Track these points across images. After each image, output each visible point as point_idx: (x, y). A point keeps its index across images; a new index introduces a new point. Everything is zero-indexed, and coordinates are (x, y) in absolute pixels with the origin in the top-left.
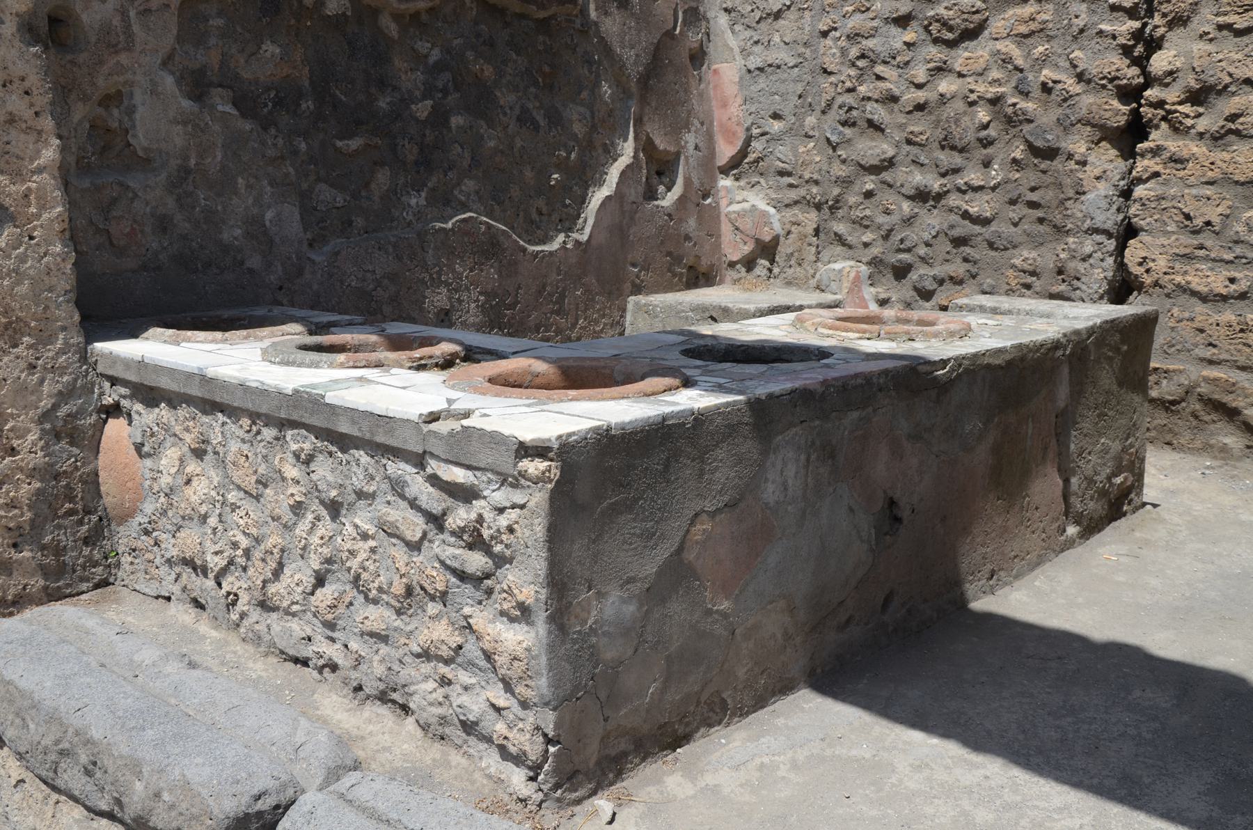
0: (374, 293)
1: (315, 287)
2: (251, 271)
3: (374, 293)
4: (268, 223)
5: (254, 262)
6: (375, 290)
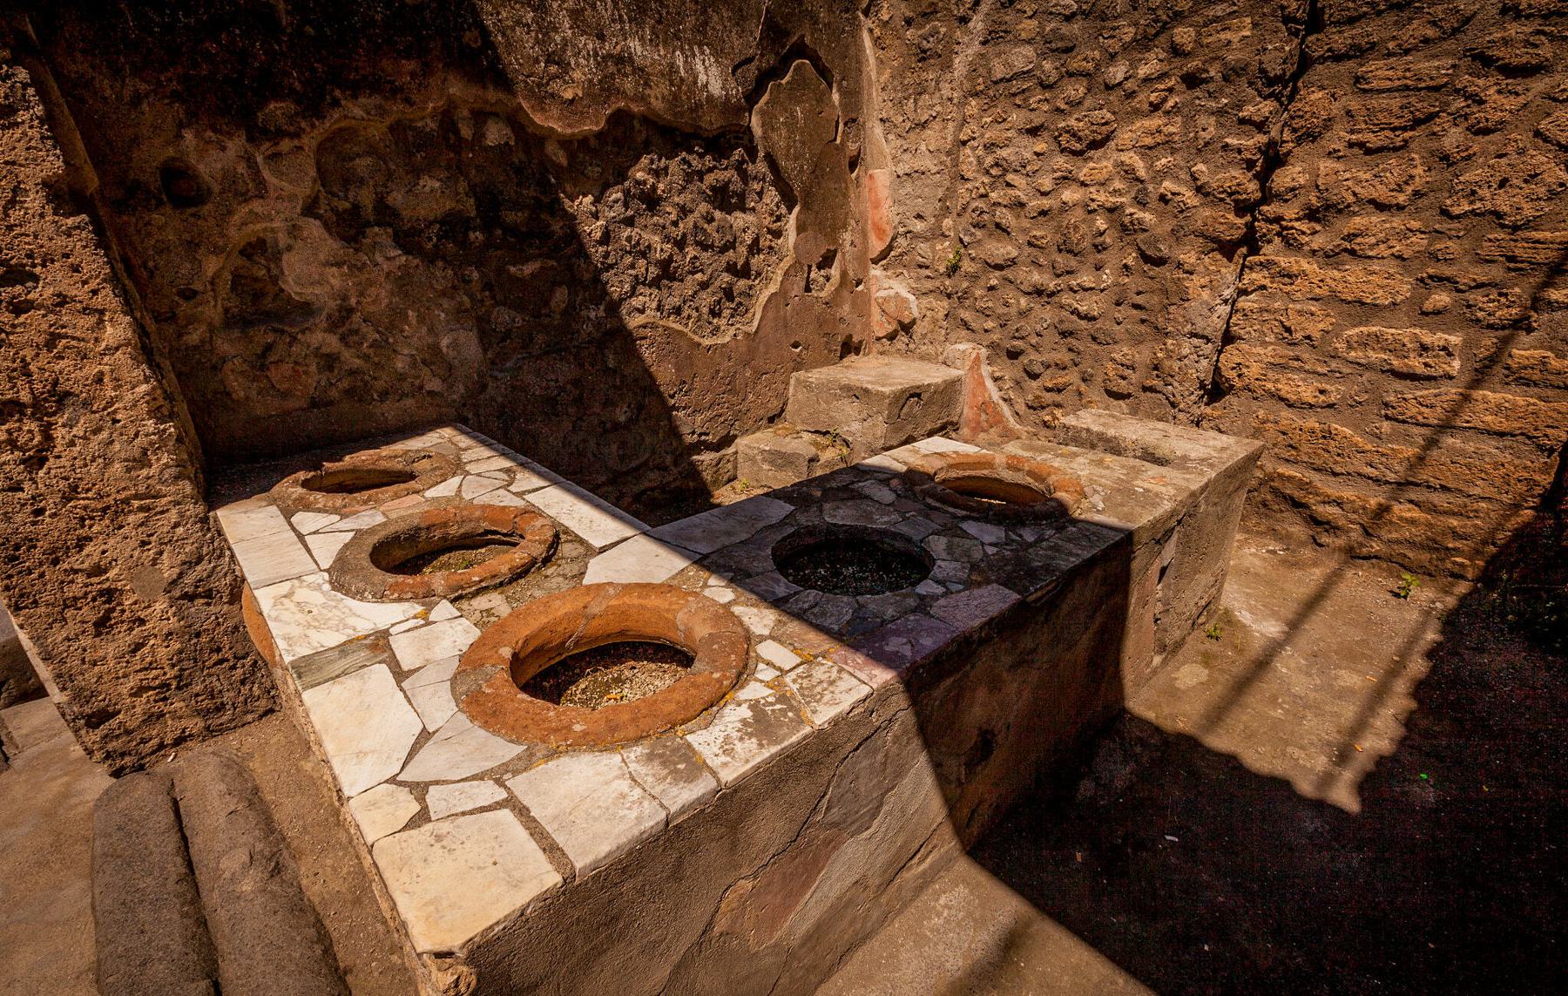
4: (444, 350)
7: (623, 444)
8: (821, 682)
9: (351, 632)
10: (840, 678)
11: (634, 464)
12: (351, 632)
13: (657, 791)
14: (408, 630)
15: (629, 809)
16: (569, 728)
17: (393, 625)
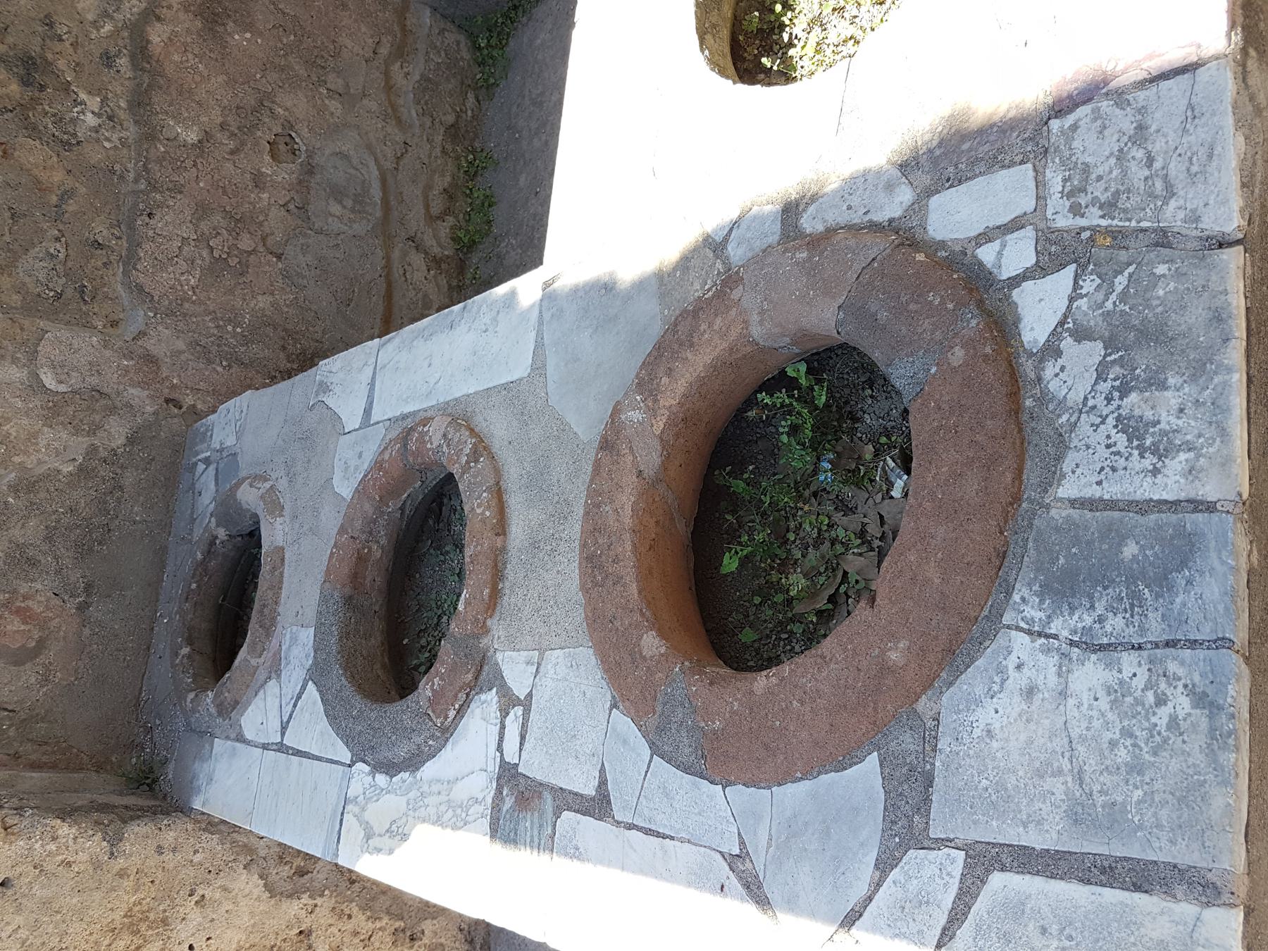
0: (216, 254)
1: (180, 345)
2: (131, 441)
3: (216, 254)
4: (62, 388)
5: (117, 432)
6: (212, 249)
7: (337, 193)
8: (1121, 156)
9: (479, 809)
10: (1142, 111)
11: (376, 193)
12: (479, 809)
13: (1156, 629)
14: (523, 738)
15: (1161, 701)
16: (885, 669)
17: (500, 748)
